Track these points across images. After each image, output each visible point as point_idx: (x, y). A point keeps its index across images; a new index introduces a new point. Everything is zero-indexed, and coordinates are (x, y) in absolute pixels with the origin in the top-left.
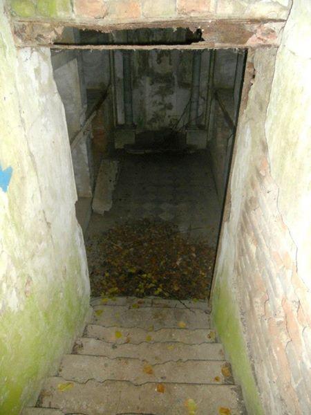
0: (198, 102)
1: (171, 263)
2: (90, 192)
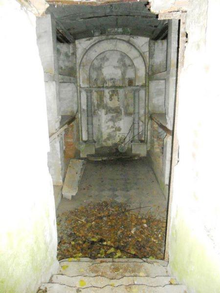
0: (139, 123)
1: (127, 232)
2: (61, 181)
